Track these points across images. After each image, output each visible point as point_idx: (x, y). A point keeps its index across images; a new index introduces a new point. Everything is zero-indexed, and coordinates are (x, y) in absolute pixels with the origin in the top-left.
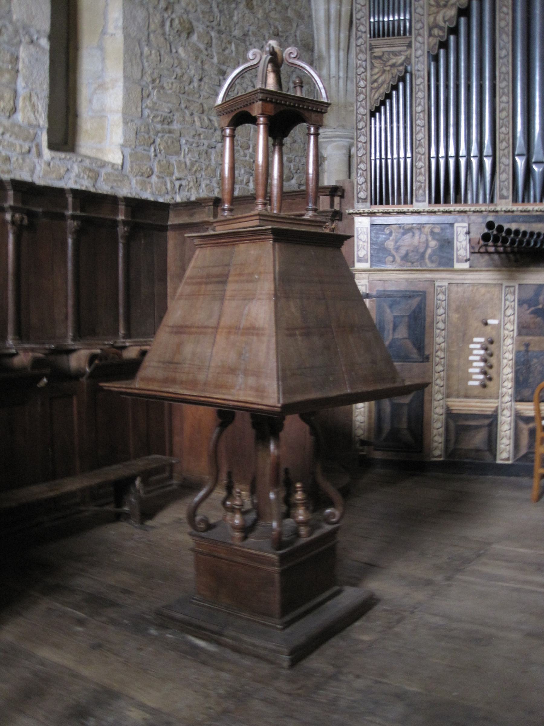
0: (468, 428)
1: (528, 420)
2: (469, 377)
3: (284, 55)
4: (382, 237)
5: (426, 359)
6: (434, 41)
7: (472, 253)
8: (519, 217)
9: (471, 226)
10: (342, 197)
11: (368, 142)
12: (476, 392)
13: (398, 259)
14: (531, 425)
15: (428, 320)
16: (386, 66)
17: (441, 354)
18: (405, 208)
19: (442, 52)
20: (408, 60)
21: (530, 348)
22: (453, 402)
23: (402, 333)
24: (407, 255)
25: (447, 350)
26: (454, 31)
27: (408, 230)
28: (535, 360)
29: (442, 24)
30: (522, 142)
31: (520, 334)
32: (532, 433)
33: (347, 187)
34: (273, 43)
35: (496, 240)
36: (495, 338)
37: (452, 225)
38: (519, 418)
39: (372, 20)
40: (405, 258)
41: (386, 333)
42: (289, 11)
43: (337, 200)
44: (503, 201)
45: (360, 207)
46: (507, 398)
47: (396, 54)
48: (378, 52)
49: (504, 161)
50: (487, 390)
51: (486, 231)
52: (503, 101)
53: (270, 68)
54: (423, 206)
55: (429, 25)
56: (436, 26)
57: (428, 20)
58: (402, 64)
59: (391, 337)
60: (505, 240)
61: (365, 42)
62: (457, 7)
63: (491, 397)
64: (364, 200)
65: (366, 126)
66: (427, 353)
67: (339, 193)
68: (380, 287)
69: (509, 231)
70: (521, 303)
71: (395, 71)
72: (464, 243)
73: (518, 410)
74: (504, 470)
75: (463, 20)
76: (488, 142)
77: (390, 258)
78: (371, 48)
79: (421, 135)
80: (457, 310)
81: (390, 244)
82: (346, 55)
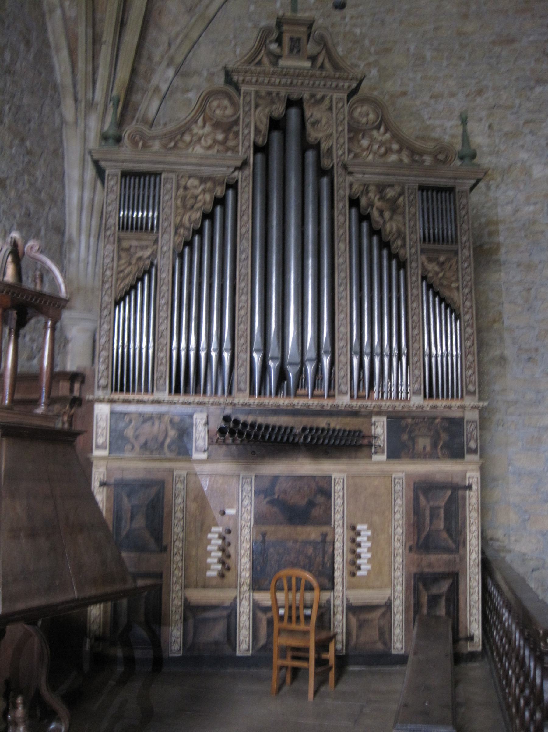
0: (206, 621)
1: (266, 610)
2: (208, 567)
3: (26, 249)
4: (121, 425)
5: (164, 549)
6: (180, 240)
7: (209, 444)
8: (256, 410)
9: (210, 417)
10: (83, 382)
11: (112, 330)
12: (214, 583)
13: (137, 447)
14: (269, 615)
15: (166, 510)
17: (179, 544)
18: (145, 397)
19: (187, 250)
20: (154, 254)
21: (267, 538)
23: (140, 522)
24: (146, 443)
25: (185, 540)
26: (200, 232)
27: (147, 419)
28: (271, 550)
29: (187, 224)
30: (260, 339)
31: (256, 522)
32: (270, 623)
33: (88, 373)
34: (15, 235)
35: (232, 433)
36: (231, 527)
37: (191, 416)
38: (257, 608)
39: (122, 213)
40: (145, 446)
41: (123, 523)
42: (43, 194)
43: (77, 386)
44: (241, 395)
45: (99, 394)
46: (245, 588)
47: (143, 248)
48: (125, 244)
49: (242, 357)
50: (226, 580)
51: (223, 424)
52: (242, 300)
53: (10, 259)
54: (164, 395)
55: (175, 226)
58: (148, 258)
59: (128, 528)
60: (241, 434)
61: (114, 234)
62: (202, 212)
63: (230, 587)
64: (105, 387)
65: (110, 313)
66: (164, 543)
67: (80, 379)
68: (118, 476)
69: (245, 424)
70: (257, 493)
71: (141, 264)
72: (203, 434)
73: (256, 601)
74: (244, 661)
75: (207, 223)
76: (227, 337)
77: (128, 447)
78: (120, 240)
79: (164, 327)
80: (195, 499)
81: (129, 432)
82: (96, 243)
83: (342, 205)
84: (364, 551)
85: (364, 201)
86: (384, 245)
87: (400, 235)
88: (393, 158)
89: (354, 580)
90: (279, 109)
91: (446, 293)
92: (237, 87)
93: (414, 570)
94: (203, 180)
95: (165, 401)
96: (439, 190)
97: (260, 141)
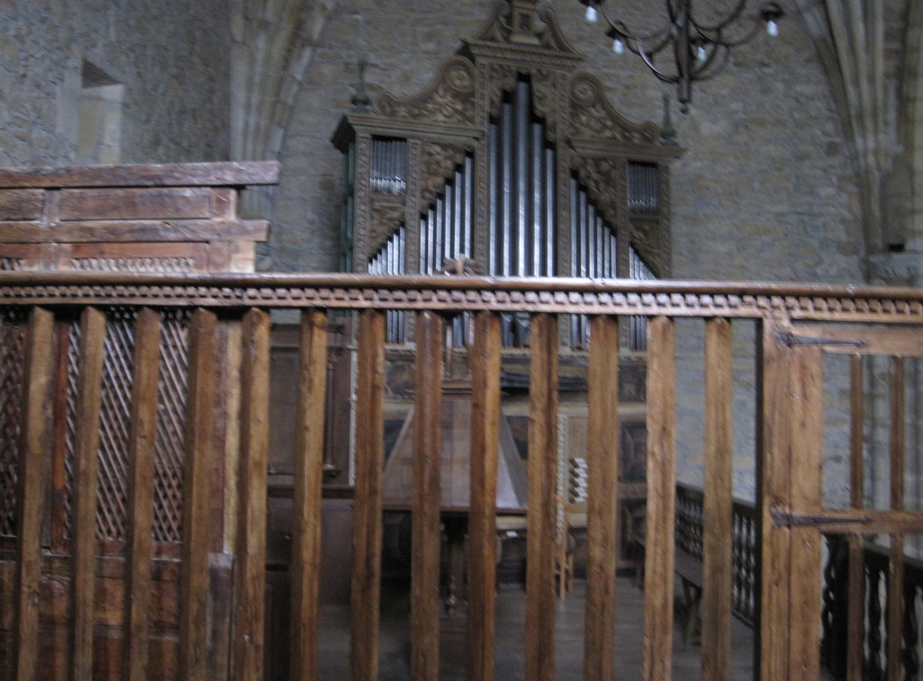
6: (425, 202)
16: (383, 218)
22: (392, 322)
26: (441, 196)
29: (432, 188)
47: (394, 209)
48: (377, 205)
56: (427, 190)
57: (421, 184)
71: (391, 225)
83: (564, 176)
84: (582, 482)
85: (583, 173)
86: (599, 213)
87: (613, 205)
88: (608, 133)
89: (572, 505)
90: (510, 82)
91: (650, 258)
92: (472, 58)
93: (622, 496)
94: (445, 147)
95: (899, 149)
96: (644, 164)
97: (495, 112)
